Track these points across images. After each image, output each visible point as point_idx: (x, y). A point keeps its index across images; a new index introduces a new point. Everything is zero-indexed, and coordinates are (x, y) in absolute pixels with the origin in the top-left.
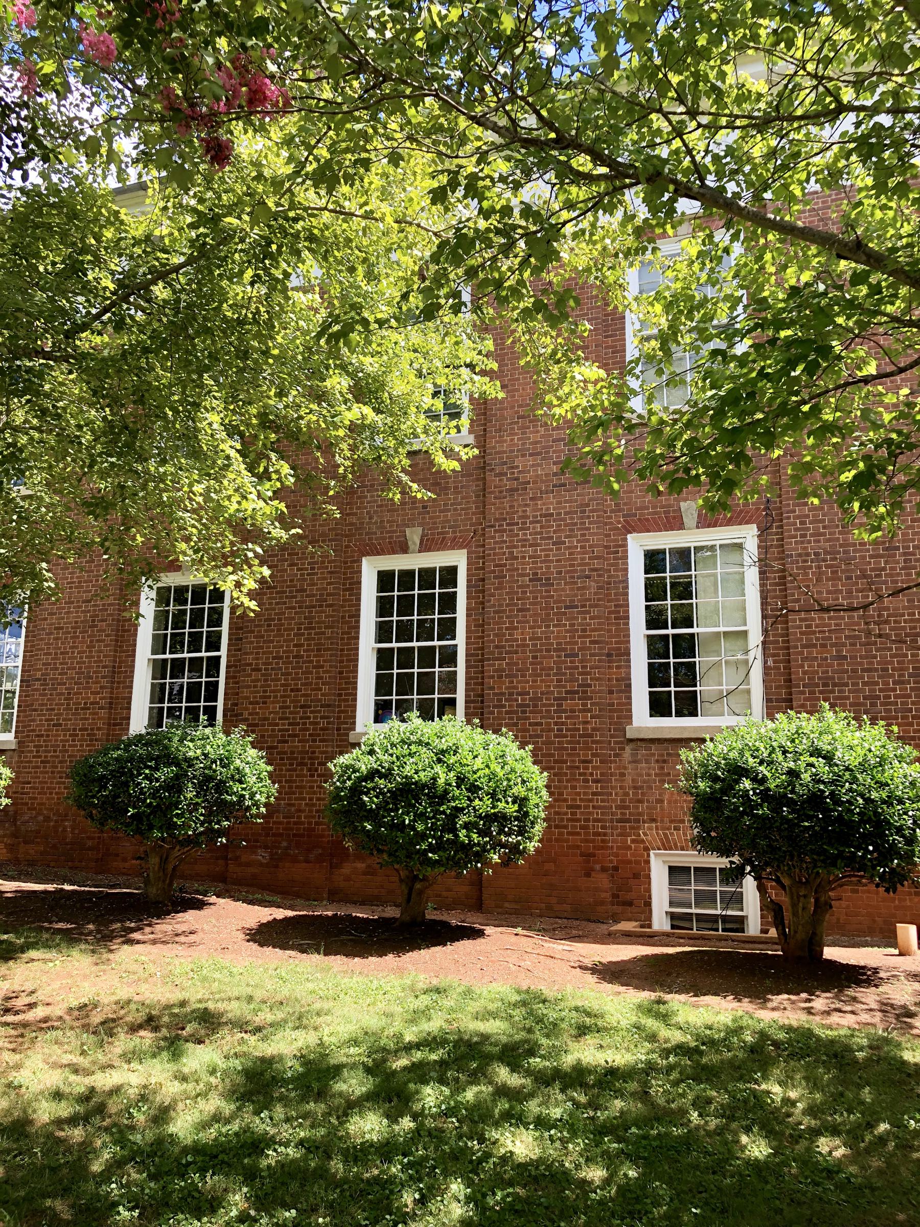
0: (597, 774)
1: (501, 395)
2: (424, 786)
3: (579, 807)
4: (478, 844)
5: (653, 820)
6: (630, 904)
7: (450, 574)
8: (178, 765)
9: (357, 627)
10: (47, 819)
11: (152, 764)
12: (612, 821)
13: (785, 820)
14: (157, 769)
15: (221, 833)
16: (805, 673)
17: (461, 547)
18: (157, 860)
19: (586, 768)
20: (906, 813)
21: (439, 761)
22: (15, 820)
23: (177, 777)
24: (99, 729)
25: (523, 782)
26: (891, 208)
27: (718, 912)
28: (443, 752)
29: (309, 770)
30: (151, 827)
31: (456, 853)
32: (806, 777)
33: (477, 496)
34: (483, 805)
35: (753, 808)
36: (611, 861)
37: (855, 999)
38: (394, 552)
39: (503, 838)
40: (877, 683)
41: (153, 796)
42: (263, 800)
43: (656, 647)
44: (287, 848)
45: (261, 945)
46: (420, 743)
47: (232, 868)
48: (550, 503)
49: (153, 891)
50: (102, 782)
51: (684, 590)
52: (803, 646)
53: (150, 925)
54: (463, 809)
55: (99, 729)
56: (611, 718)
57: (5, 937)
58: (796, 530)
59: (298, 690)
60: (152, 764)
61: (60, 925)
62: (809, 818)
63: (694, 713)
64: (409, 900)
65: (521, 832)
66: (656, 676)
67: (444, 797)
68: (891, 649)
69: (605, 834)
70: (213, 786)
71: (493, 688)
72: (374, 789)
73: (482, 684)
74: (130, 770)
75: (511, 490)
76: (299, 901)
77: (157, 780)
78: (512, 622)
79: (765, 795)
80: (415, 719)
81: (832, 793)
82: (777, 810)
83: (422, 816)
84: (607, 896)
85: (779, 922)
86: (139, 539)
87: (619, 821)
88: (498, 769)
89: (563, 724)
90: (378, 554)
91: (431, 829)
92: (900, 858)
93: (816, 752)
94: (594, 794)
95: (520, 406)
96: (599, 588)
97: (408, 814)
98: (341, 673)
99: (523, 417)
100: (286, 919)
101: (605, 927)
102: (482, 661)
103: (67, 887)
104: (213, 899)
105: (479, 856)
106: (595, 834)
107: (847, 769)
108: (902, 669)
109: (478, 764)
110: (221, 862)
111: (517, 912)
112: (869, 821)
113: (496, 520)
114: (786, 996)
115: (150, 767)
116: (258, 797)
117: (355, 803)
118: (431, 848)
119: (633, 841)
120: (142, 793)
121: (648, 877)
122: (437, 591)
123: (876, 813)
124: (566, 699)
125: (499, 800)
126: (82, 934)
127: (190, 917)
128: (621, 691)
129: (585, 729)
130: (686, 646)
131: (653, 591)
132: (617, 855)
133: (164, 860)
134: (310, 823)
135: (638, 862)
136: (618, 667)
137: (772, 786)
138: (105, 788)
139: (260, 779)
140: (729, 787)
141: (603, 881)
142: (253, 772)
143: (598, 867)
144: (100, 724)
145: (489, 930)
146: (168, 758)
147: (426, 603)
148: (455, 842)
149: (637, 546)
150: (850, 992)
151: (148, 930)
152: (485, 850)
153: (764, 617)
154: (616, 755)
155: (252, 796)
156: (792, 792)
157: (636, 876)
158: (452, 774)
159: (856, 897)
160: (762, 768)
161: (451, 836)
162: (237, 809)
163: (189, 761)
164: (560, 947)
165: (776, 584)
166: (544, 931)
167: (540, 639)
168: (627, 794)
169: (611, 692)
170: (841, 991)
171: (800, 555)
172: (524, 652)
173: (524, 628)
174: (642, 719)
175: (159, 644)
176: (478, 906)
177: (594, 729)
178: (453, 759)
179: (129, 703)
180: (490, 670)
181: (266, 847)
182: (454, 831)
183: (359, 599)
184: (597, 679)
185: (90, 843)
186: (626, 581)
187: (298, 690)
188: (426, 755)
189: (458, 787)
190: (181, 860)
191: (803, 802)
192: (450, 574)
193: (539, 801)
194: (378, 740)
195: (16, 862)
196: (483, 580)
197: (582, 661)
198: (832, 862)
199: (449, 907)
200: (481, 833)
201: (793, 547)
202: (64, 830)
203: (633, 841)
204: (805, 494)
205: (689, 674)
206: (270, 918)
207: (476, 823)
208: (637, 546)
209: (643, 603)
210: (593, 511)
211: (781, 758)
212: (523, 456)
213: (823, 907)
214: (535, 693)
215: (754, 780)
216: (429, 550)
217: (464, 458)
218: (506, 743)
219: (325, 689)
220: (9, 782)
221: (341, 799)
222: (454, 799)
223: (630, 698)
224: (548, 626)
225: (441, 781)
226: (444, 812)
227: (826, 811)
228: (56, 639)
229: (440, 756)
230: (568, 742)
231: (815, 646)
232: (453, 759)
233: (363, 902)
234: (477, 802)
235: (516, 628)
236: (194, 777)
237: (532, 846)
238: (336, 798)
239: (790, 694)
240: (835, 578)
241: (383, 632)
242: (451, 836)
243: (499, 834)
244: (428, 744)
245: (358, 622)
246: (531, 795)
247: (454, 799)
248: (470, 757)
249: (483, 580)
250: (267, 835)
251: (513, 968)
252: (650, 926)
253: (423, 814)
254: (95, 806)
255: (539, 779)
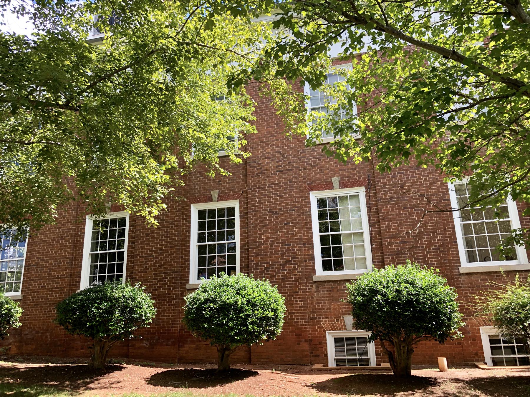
0: (301, 298)
1: (256, 132)
2: (232, 305)
3: (294, 313)
4: (257, 331)
5: (327, 318)
6: (318, 356)
7: (231, 211)
8: (111, 301)
9: (189, 236)
10: (37, 332)
11: (99, 301)
12: (308, 319)
13: (397, 312)
14: (101, 304)
15: (131, 333)
16: (389, 249)
17: (236, 199)
18: (99, 348)
19: (296, 295)
20: (447, 307)
21: (238, 294)
22: (21, 334)
23: (111, 307)
24: (65, 287)
25: (275, 302)
26: (448, 44)
27: (358, 357)
28: (239, 289)
29: (168, 302)
30: (98, 332)
31: (247, 336)
32: (405, 293)
33: (243, 176)
34: (259, 313)
35: (381, 308)
36: (309, 337)
37: (432, 392)
38: (206, 202)
39: (268, 328)
40: (420, 253)
41: (100, 317)
42: (151, 316)
43: (324, 240)
44: (158, 340)
45: (155, 385)
46: (228, 286)
47: (131, 350)
48: (276, 179)
49: (96, 363)
50: (74, 311)
51: (334, 215)
52: (388, 238)
53: (97, 380)
54: (250, 315)
55: (65, 287)
56: (306, 272)
57: (25, 390)
58: (382, 188)
59: (162, 265)
60: (99, 301)
61: (51, 383)
62: (407, 311)
63: (342, 269)
64: (222, 360)
65: (275, 325)
66: (325, 252)
67: (241, 310)
68: (424, 238)
69: (306, 325)
70: (128, 311)
71: (253, 261)
72: (208, 308)
73: (248, 259)
74: (88, 305)
75: (259, 173)
76: (164, 364)
77: (101, 309)
78: (260, 231)
79: (387, 302)
80: (225, 276)
81: (417, 300)
82: (392, 308)
83: (231, 320)
84: (308, 353)
85: (391, 360)
86: (104, 191)
87: (311, 319)
88: (264, 296)
89: (285, 276)
90: (198, 202)
91: (235, 325)
92: (446, 327)
93: (407, 282)
94: (300, 307)
95: (260, 138)
96: (299, 215)
97: (225, 319)
98: (182, 257)
99: (262, 142)
100: (163, 372)
101: (308, 367)
102: (248, 249)
103: (50, 365)
104: (125, 365)
105: (257, 337)
106: (301, 325)
107: (421, 288)
108: (429, 246)
109: (256, 294)
110: (125, 348)
111: (267, 363)
112: (432, 311)
113: (252, 186)
114: (403, 393)
115: (98, 303)
116: (148, 315)
117: (199, 315)
118: (237, 334)
119: (318, 327)
120: (94, 315)
121: (326, 343)
122: (226, 218)
123: (435, 307)
124: (286, 265)
125: (266, 310)
126: (63, 387)
127: (116, 374)
128: (310, 260)
129: (295, 278)
130: (337, 239)
131: (322, 215)
132: (311, 334)
133: (102, 348)
134: (168, 327)
135: (321, 337)
136: (308, 250)
137: (390, 297)
138: (75, 314)
139: (150, 307)
140: (370, 300)
141: (306, 346)
142: (146, 304)
143: (303, 340)
144: (65, 285)
145: (259, 372)
146: (105, 298)
147: (221, 225)
148: (247, 331)
149: (314, 197)
150: (429, 389)
151: (96, 382)
152: (260, 334)
153: (370, 226)
154: (309, 289)
155: (146, 314)
156: (399, 300)
157: (320, 343)
158: (245, 299)
159: (424, 345)
160: (385, 290)
161: (245, 328)
162: (138, 321)
163: (117, 299)
164: (293, 377)
165: (374, 212)
166: (285, 371)
167: (273, 238)
168: (315, 306)
169: (306, 261)
170: (425, 389)
171: (384, 199)
172: (266, 244)
173: (266, 233)
174: (320, 273)
175: (94, 247)
176: (249, 361)
177: (299, 278)
178: (244, 293)
179: (80, 275)
180: (251, 253)
181: (148, 340)
182: (246, 326)
183: (190, 223)
184: (300, 255)
185: (59, 343)
186: (310, 212)
187: (162, 265)
188: (231, 291)
189: (247, 305)
190: (110, 347)
191: (404, 304)
192: (231, 211)
193: (282, 309)
194: (201, 286)
195: (22, 354)
196: (247, 213)
197: (292, 247)
198: (417, 330)
199: (235, 363)
200: (258, 326)
201: (380, 195)
202: (46, 337)
203: (318, 327)
204: (421, 163)
205: (338, 252)
206: (156, 372)
207: (256, 322)
208: (314, 197)
209: (318, 221)
210: (295, 182)
211: (392, 285)
212: (263, 159)
213: (410, 351)
214: (272, 262)
215: (382, 295)
216: (222, 200)
217: (245, 157)
218: (266, 285)
219: (175, 264)
220: (20, 315)
221: (192, 313)
222: (246, 311)
223: (314, 263)
224: (277, 232)
225: (239, 303)
226: (241, 317)
227: (414, 307)
228: (44, 246)
229: (238, 291)
230: (288, 284)
231: (392, 238)
232: (244, 293)
233: (195, 363)
234: (256, 312)
235: (263, 234)
236: (119, 306)
237: (279, 331)
238: (189, 312)
239: (383, 259)
240: (399, 208)
241: (201, 238)
242: (245, 328)
243: (266, 326)
244: (232, 286)
245: (190, 233)
246: (279, 308)
247: (246, 311)
248: (252, 291)
249: (247, 213)
250: (148, 334)
251: (277, 388)
252: (327, 366)
253: (232, 319)
254: (70, 323)
255: (281, 300)
